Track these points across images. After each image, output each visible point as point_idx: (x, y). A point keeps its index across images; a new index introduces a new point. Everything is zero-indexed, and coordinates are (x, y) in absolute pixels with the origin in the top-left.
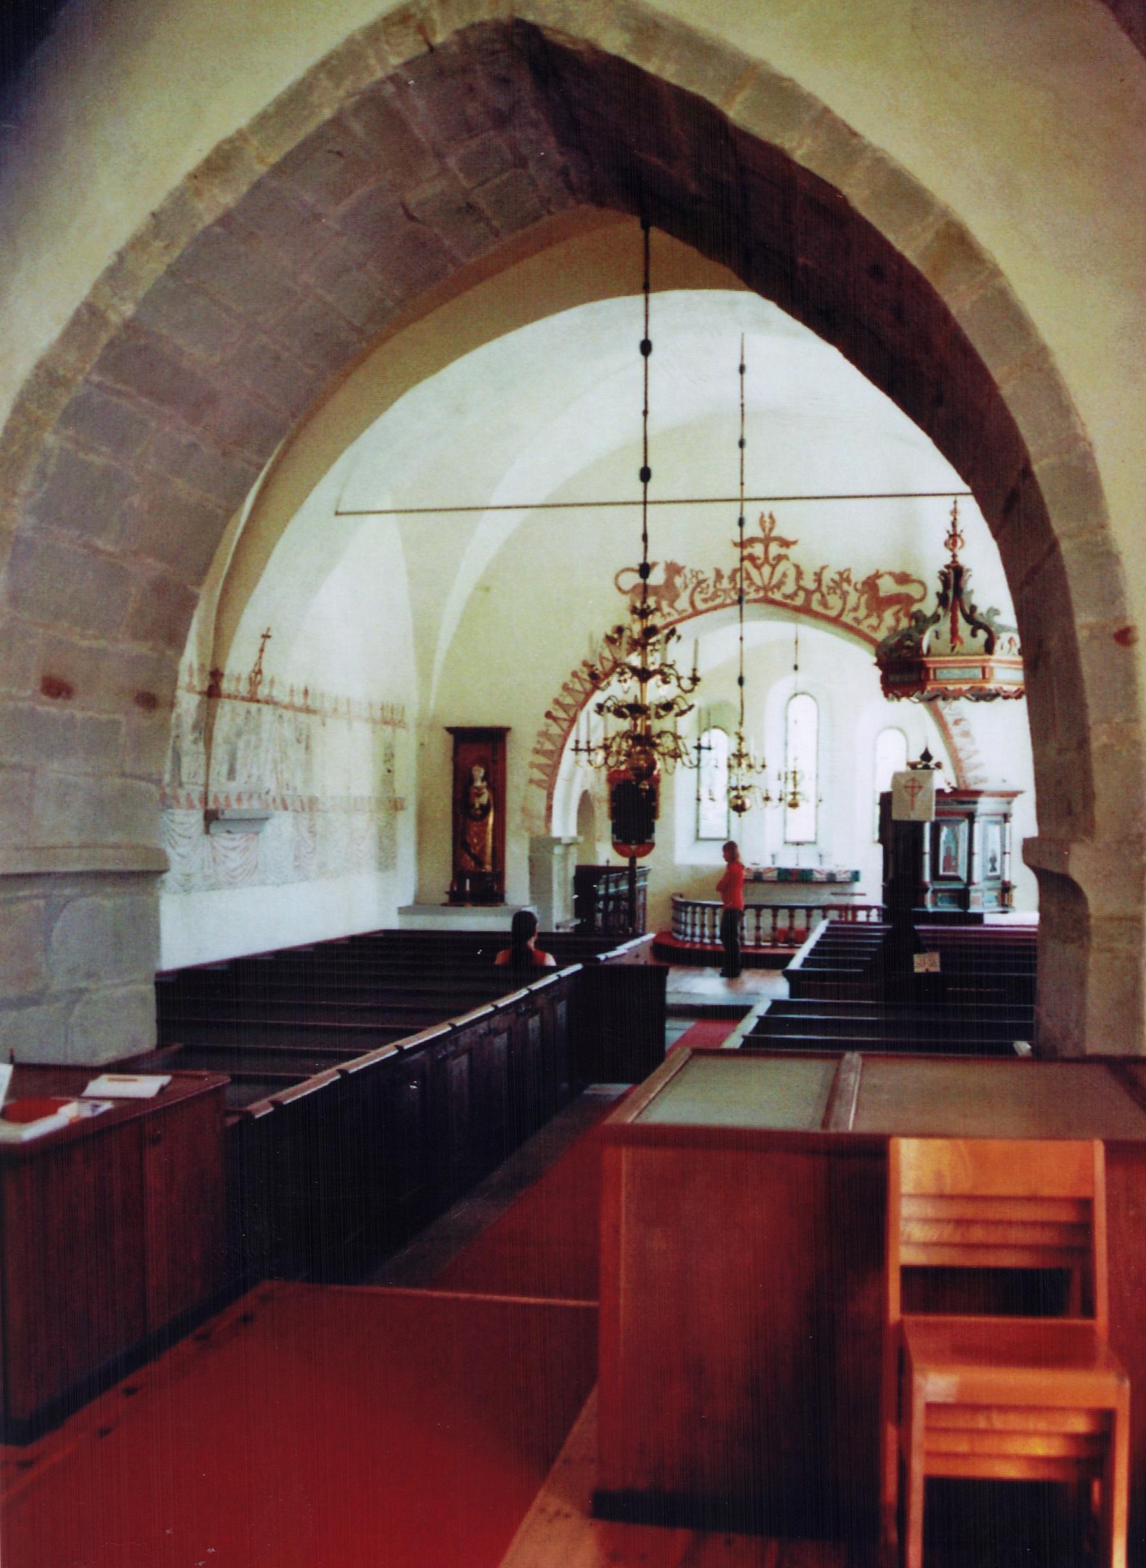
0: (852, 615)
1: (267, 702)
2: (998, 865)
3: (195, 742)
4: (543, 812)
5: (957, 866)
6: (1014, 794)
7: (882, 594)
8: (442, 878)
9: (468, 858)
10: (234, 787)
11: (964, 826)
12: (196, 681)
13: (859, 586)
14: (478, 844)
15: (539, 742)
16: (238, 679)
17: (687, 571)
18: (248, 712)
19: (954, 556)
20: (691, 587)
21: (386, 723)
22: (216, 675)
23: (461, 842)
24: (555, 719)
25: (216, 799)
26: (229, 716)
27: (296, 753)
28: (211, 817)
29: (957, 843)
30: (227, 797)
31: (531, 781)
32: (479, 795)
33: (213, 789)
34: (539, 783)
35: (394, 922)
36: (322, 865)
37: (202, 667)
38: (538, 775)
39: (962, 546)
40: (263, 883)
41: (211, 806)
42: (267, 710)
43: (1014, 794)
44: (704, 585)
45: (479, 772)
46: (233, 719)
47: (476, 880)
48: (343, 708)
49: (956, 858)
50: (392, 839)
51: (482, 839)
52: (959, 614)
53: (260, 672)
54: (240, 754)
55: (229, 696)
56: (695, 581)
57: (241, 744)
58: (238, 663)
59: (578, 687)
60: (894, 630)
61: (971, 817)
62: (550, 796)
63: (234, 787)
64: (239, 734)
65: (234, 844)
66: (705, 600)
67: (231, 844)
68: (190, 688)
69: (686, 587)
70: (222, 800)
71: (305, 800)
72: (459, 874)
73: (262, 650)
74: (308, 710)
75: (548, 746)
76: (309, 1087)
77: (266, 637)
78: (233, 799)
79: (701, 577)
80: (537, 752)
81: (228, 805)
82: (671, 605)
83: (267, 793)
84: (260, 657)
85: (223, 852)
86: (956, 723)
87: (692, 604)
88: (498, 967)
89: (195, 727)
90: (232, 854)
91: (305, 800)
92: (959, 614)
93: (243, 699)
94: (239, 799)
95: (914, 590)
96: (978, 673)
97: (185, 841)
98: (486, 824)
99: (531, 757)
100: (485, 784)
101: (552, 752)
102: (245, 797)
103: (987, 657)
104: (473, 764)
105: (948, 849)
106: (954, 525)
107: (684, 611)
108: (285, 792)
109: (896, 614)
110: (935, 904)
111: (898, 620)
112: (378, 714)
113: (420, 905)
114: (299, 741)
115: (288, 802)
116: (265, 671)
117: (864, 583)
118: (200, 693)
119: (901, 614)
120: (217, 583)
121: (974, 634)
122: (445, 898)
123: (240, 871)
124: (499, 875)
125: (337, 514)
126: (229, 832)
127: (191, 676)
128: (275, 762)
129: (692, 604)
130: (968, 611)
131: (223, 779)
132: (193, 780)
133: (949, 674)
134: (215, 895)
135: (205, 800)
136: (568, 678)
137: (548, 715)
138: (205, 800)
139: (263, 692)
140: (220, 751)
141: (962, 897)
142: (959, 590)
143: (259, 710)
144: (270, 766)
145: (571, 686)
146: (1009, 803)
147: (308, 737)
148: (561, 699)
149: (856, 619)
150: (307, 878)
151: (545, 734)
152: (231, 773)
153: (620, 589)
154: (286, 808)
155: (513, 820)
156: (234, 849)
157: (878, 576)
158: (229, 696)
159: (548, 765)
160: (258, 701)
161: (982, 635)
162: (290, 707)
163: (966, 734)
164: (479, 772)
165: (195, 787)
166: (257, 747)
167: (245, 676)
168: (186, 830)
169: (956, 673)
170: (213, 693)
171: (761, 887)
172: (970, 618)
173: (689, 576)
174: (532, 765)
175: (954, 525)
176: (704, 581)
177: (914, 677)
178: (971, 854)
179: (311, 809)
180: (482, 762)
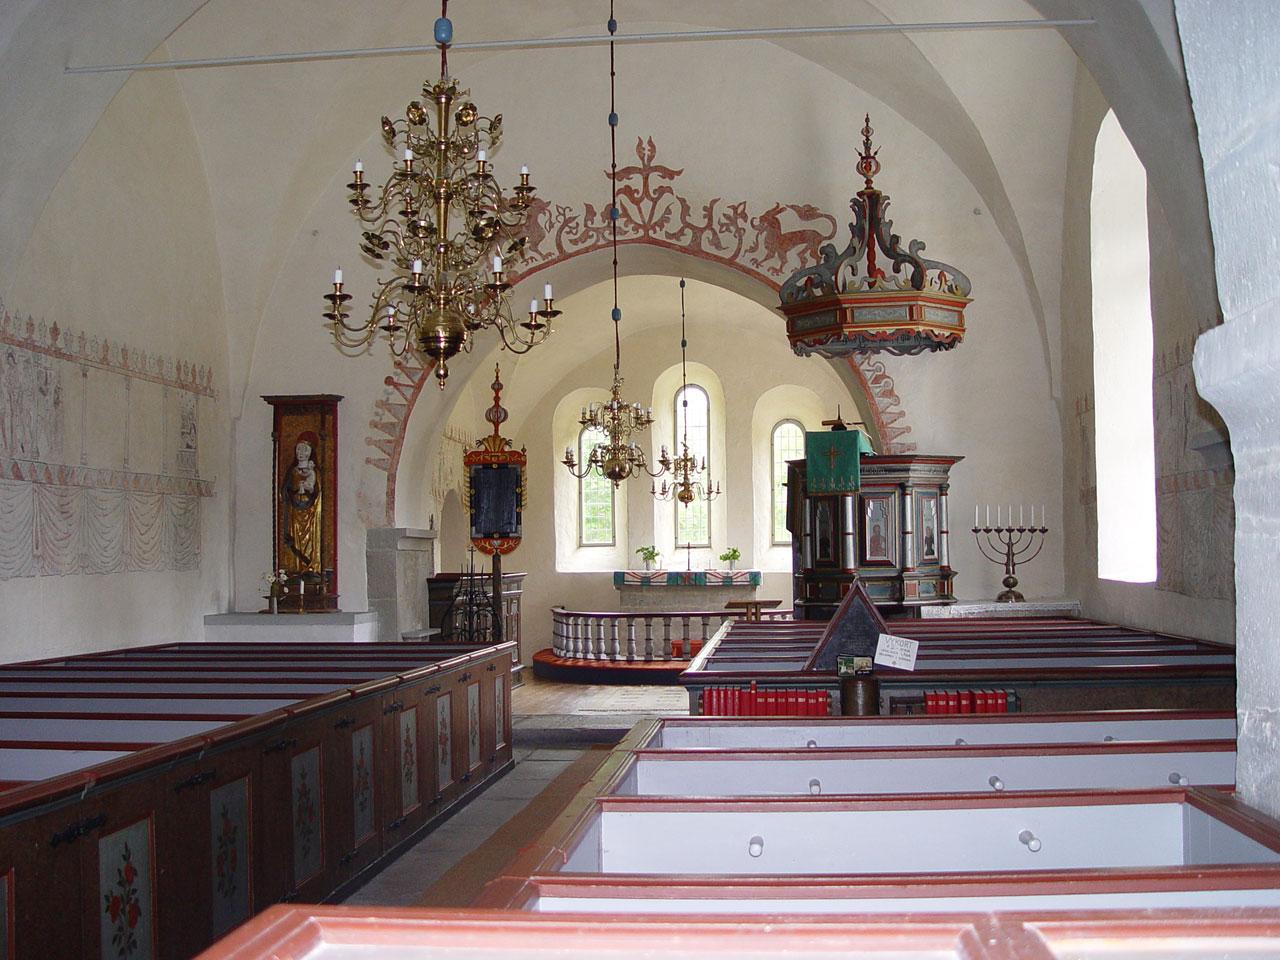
2: (935, 547)
4: (384, 498)
6: (951, 461)
11: (895, 499)
13: (757, 222)
15: (377, 414)
17: (552, 208)
19: (868, 182)
20: (557, 226)
24: (396, 385)
31: (368, 461)
32: (304, 479)
34: (378, 464)
43: (951, 461)
45: (304, 450)
47: (306, 586)
52: (877, 248)
56: (561, 219)
61: (902, 487)
66: (575, 242)
69: (552, 226)
75: (388, 418)
86: (877, 380)
87: (559, 246)
92: (877, 248)
95: (821, 226)
103: (915, 293)
104: (301, 438)
105: (876, 529)
106: (867, 145)
107: (550, 254)
109: (801, 254)
111: (804, 261)
117: (763, 219)
119: (807, 255)
121: (897, 270)
129: (559, 246)
133: (869, 319)
141: (897, 584)
149: (754, 261)
151: (384, 404)
157: (778, 210)
159: (389, 442)
161: (908, 269)
163: (890, 393)
171: (650, 595)
172: (891, 249)
174: (369, 441)
175: (867, 145)
177: (828, 319)
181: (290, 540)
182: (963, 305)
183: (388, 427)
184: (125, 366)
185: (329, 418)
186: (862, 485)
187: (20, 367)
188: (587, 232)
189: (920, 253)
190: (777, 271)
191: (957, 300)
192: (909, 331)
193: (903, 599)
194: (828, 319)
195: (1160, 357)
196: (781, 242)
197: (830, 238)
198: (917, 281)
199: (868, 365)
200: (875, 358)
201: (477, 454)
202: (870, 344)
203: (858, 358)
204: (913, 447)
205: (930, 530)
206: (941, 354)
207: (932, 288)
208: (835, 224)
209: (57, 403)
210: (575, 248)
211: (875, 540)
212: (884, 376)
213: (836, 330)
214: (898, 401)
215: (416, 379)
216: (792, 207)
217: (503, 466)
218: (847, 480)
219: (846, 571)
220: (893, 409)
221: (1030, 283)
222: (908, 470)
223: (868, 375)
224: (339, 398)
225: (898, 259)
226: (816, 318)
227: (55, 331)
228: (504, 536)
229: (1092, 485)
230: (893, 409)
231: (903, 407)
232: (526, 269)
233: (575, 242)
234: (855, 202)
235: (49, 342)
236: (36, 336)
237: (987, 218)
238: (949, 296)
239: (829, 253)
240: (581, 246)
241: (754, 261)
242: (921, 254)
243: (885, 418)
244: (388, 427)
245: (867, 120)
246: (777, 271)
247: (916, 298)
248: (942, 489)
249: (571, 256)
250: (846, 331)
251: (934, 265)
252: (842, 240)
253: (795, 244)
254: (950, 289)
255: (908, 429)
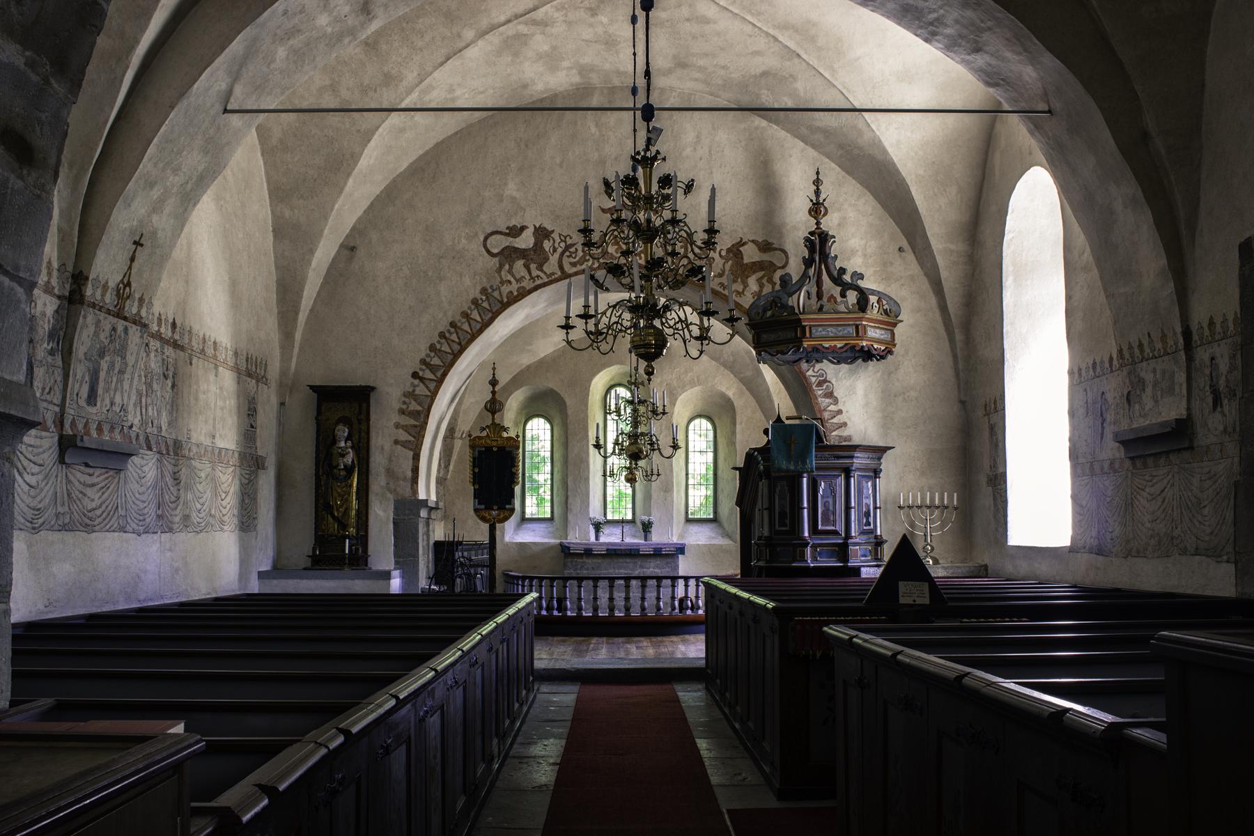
0: (718, 280)
1: (134, 323)
2: (871, 520)
3: (52, 353)
4: (409, 474)
5: (835, 521)
6: (884, 450)
7: (746, 260)
8: (303, 543)
9: (330, 519)
10: (95, 413)
11: (841, 481)
12: (54, 282)
13: (724, 253)
14: (341, 506)
15: (404, 403)
16: (105, 287)
17: (555, 236)
18: (114, 329)
19: (818, 223)
20: (560, 250)
21: (250, 375)
22: (78, 279)
23: (323, 506)
24: (422, 379)
25: (73, 423)
26: (92, 329)
27: (162, 390)
28: (68, 446)
29: (834, 497)
30: (86, 424)
31: (396, 442)
32: (343, 456)
33: (70, 412)
34: (404, 444)
35: (254, 587)
36: (187, 517)
37: (62, 266)
38: (403, 436)
39: (825, 214)
40: (123, 529)
41: (68, 430)
42: (134, 331)
43: (884, 450)
44: (572, 250)
45: (342, 431)
46: (96, 334)
47: (337, 544)
48: (210, 352)
49: (834, 513)
50: (254, 499)
51: (346, 501)
52: (825, 276)
53: (129, 284)
54: (102, 375)
55: (94, 305)
56: (563, 245)
57: (104, 365)
58: (106, 266)
59: (446, 348)
60: (758, 295)
61: (847, 472)
62: (416, 458)
63: (95, 413)
64: (102, 354)
65: (94, 480)
66: (574, 265)
67: (89, 480)
68: (48, 289)
69: (555, 250)
70: (80, 427)
71: (170, 443)
72: (321, 539)
73: (132, 259)
74: (176, 345)
75: (414, 406)
76: (367, 715)
77: (138, 244)
78: (93, 426)
79: (569, 241)
80: (402, 412)
81: (88, 433)
82: (540, 268)
83: (131, 427)
84: (130, 268)
85: (81, 487)
86: (820, 384)
87: (561, 267)
88: (459, 595)
89: (52, 335)
90: (89, 492)
91: (170, 443)
92: (825, 276)
93: (109, 312)
94: (99, 429)
95: (776, 259)
96: (852, 330)
97: (36, 469)
98: (351, 486)
99: (396, 418)
100: (349, 443)
101: (418, 412)
102: (106, 428)
103: (861, 315)
104: (337, 423)
105: (825, 504)
106: (817, 193)
107: (553, 274)
108: (149, 430)
109: (759, 280)
110: (814, 559)
111: (761, 286)
112: (243, 366)
113: (279, 569)
114: (166, 377)
115: (153, 442)
116: (133, 285)
117: (729, 250)
118: (59, 297)
119: (764, 281)
120: (21, 365)
121: (843, 295)
122: (305, 562)
123: (98, 512)
124: (362, 539)
125: (226, 111)
126: (87, 465)
127: (49, 274)
128: (140, 395)
129: (561, 267)
130: (835, 273)
131: (82, 403)
132: (49, 398)
133: (823, 333)
134: (68, 537)
135: (60, 422)
136: (436, 339)
137: (415, 375)
138: (60, 422)
139: (132, 308)
140: (79, 370)
141: (842, 551)
142: (825, 257)
143: (126, 329)
144: (134, 398)
145: (438, 346)
146: (879, 459)
147: (175, 375)
148: (428, 360)
149: (722, 284)
150: (171, 530)
151: (410, 395)
152: (92, 398)
153: (488, 251)
154: (150, 449)
155: (378, 483)
156: (93, 485)
157: (741, 243)
158: (94, 305)
159: (415, 426)
160: (125, 319)
161: (852, 297)
162: (158, 336)
163: (830, 395)
164: (342, 431)
165: (51, 407)
166: (121, 372)
167: (112, 284)
168: (38, 454)
169: (831, 331)
170: (74, 297)
171: (589, 561)
172: (837, 279)
173: (558, 240)
174: (397, 426)
175: (817, 193)
176: (572, 245)
177: (790, 335)
178: (848, 508)
179: (176, 454)
180: (345, 421)
181: (329, 508)
182: (895, 325)
183: (415, 415)
184: (215, 357)
185: (364, 405)
186: (817, 469)
187: (152, 355)
188: (584, 256)
189: (859, 282)
190: (739, 294)
191: (891, 318)
192: (853, 347)
193: (847, 561)
194: (790, 335)
195: (1076, 370)
196: (742, 270)
197: (783, 267)
198: (863, 304)
199: (812, 372)
200: (818, 366)
201: (480, 438)
202: (817, 354)
203: (804, 365)
204: (849, 438)
205: (868, 506)
206: (872, 364)
207: (874, 312)
208: (787, 257)
209: (173, 386)
210: (574, 270)
211: (825, 514)
212: (825, 381)
213: (797, 342)
214: (836, 401)
215: (439, 374)
216: (753, 241)
217: (502, 449)
218: (804, 462)
219: (803, 539)
220: (832, 408)
221: (943, 308)
222: (852, 457)
223: (813, 379)
224: (373, 389)
225: (845, 287)
226: (777, 332)
227: (174, 325)
228: (502, 508)
229: (1001, 470)
230: (832, 408)
231: (840, 406)
232: (532, 285)
233: (574, 265)
234: (807, 239)
235: (170, 334)
236: (163, 330)
237: (910, 256)
238: (884, 318)
239: (785, 280)
240: (579, 268)
241: (722, 284)
242: (859, 282)
243: (826, 415)
244: (415, 415)
245: (818, 173)
246: (739, 294)
247: (861, 319)
248: (876, 473)
249: (570, 276)
250: (805, 344)
251: (873, 292)
252: (795, 268)
253: (754, 272)
254: (886, 311)
255: (845, 424)
